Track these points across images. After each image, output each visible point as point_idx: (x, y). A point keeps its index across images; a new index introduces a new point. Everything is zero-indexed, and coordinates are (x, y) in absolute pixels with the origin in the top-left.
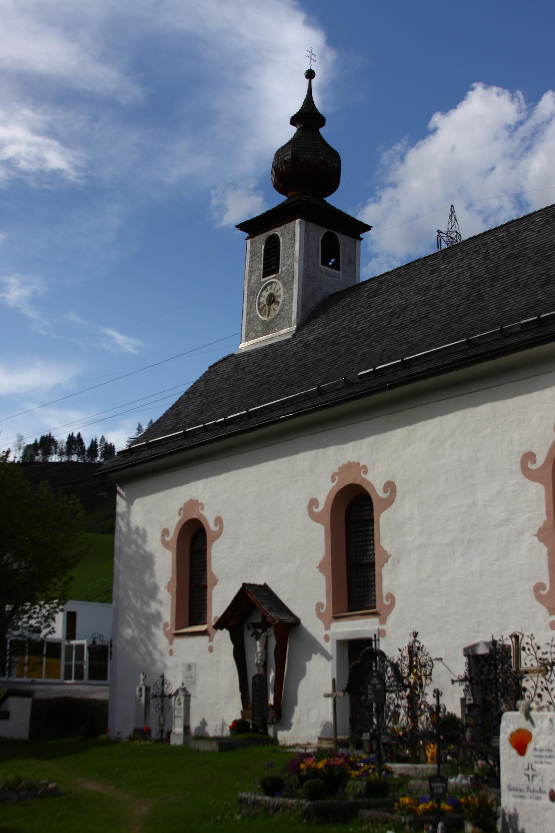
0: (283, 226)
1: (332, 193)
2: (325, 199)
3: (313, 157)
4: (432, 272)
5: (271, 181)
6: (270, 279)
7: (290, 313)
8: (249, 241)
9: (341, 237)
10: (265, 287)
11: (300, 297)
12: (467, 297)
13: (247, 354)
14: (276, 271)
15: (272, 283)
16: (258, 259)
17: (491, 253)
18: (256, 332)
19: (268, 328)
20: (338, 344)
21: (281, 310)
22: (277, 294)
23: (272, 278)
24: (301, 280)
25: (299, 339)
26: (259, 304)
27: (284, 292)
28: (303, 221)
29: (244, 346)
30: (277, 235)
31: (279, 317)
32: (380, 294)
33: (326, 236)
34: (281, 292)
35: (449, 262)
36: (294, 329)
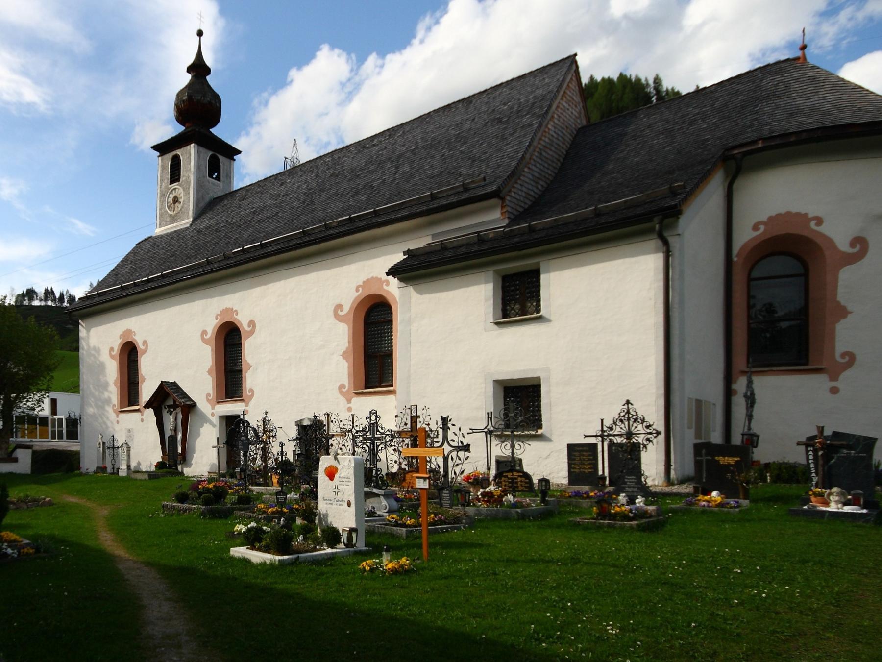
4: (281, 185)
9: (221, 158)
12: (304, 203)
14: (178, 180)
19: (174, 219)
21: (182, 207)
29: (159, 231)
33: (212, 157)
34: (182, 195)
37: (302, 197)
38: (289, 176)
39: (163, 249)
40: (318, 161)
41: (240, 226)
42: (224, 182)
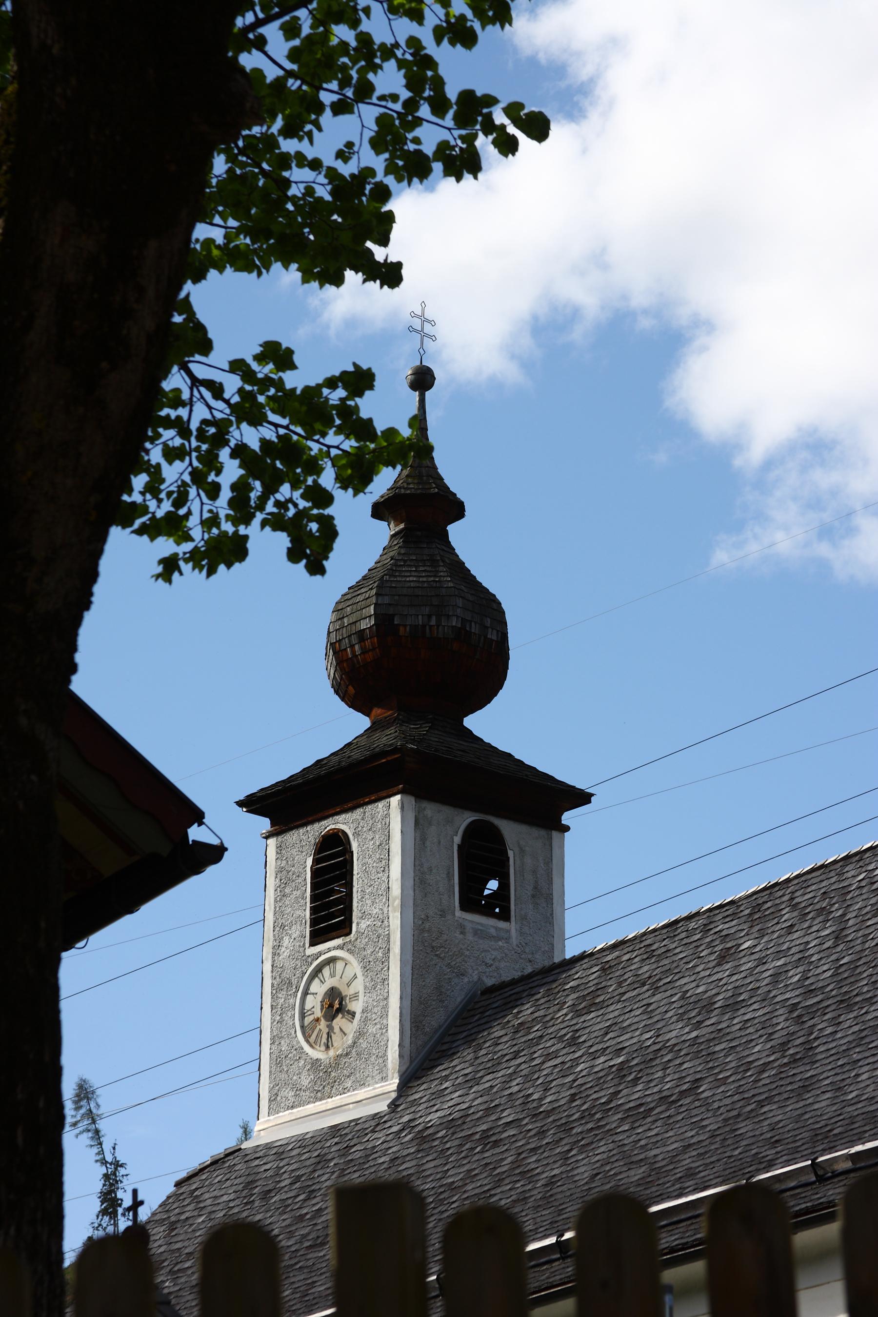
0: (359, 811)
1: (507, 658)
2: (472, 722)
3: (433, 622)
4: (723, 958)
5: (326, 673)
6: (329, 950)
7: (381, 1043)
8: (272, 842)
9: (511, 832)
10: (318, 970)
11: (408, 1003)
12: (784, 1046)
13: (277, 1152)
14: (343, 928)
15: (332, 960)
16: (299, 893)
17: (851, 923)
18: (298, 1090)
19: (327, 1079)
20: (496, 1144)
21: (360, 1034)
22: (345, 991)
23: (335, 948)
24: (409, 957)
25: (405, 1119)
26: (303, 1016)
27: (365, 987)
28: (410, 800)
29: (272, 1128)
30: (339, 830)
31: (354, 1053)
32: (601, 1006)
33: (471, 832)
34: (359, 986)
35: (762, 934)
36: (394, 1087)
37: (781, 1021)
38: (751, 920)
39: (284, 1206)
40: (850, 870)
41: (566, 1128)
42: (523, 918)
